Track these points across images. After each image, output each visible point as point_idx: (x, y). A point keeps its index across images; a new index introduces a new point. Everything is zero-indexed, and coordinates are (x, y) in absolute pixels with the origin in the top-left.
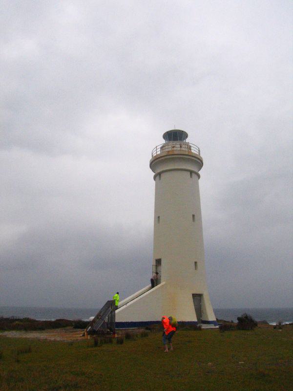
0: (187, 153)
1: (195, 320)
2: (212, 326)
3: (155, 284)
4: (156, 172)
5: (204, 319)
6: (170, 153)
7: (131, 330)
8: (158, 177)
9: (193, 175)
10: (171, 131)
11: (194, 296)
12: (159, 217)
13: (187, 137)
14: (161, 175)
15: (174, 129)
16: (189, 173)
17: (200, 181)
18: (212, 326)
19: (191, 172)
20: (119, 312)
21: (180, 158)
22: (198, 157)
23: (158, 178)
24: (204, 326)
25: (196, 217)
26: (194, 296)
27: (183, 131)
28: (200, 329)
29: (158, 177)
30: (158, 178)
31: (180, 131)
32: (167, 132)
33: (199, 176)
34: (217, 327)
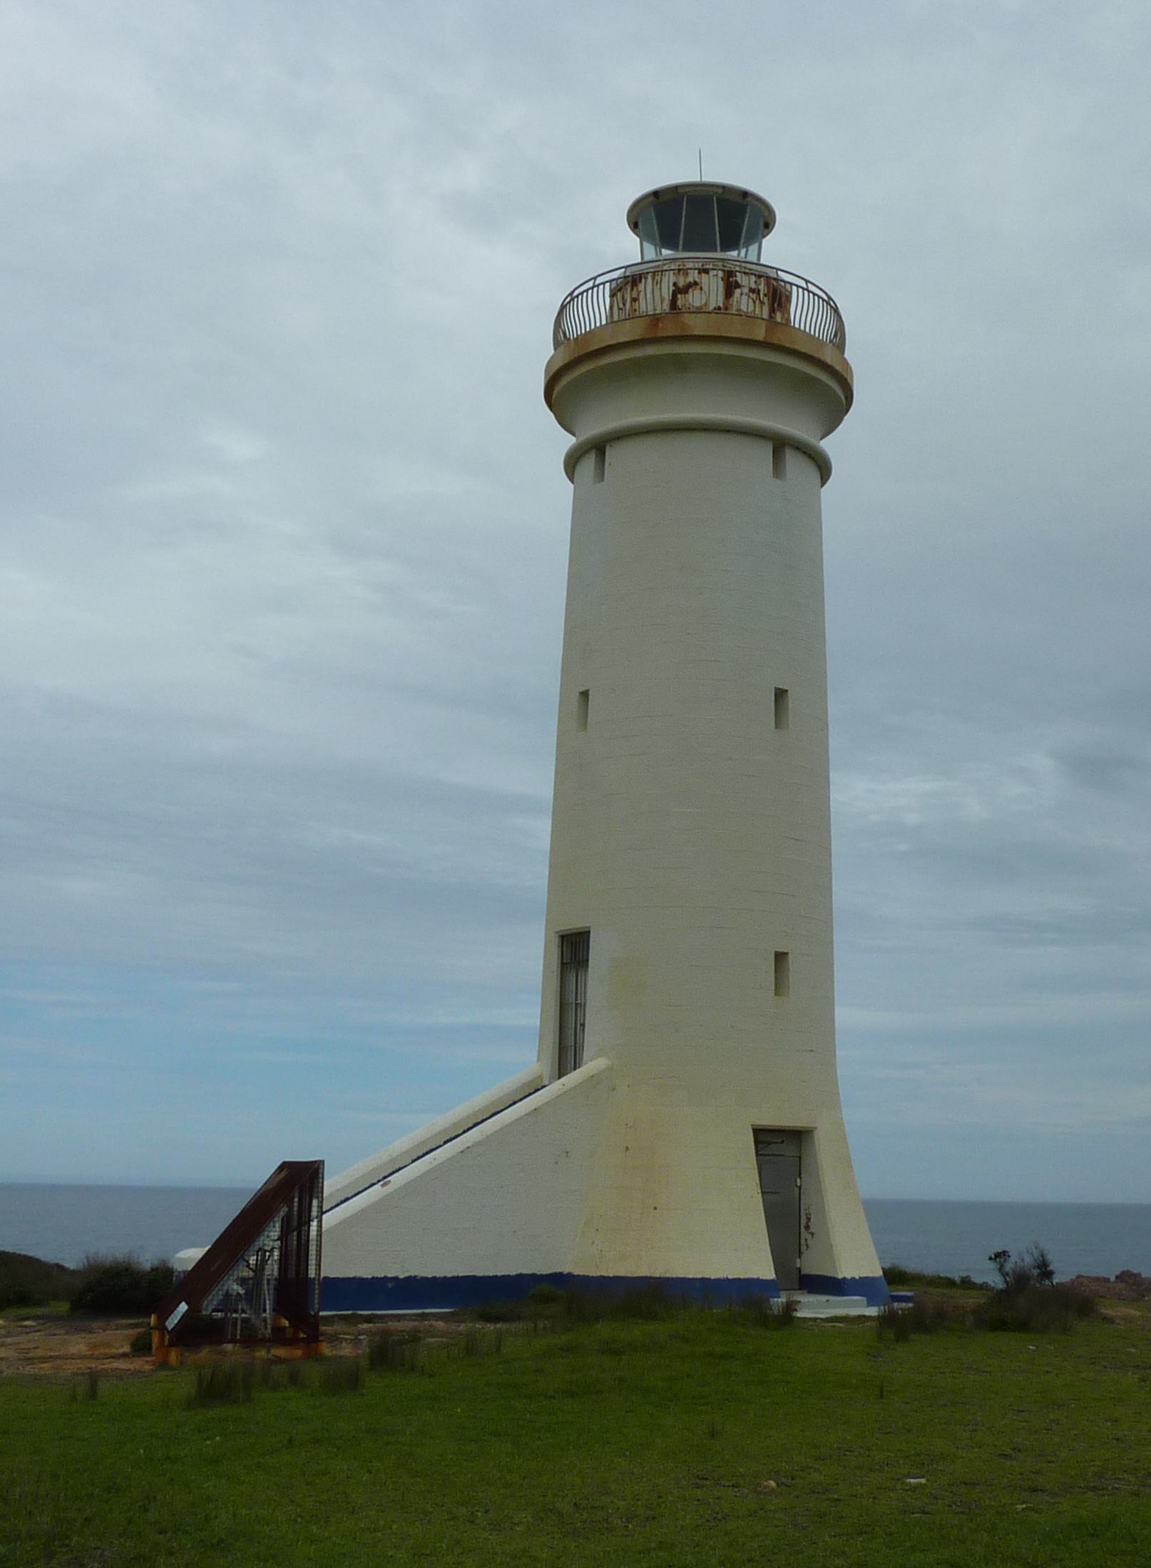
0: (760, 334)
1: (767, 1271)
2: (856, 1307)
3: (577, 1066)
4: (583, 437)
5: (811, 1265)
6: (668, 329)
7: (402, 1317)
8: (589, 463)
9: (793, 461)
10: (675, 189)
11: (763, 1136)
12: (585, 695)
13: (768, 225)
14: (610, 453)
15: (694, 178)
16: (764, 452)
17: (828, 492)
18: (856, 1307)
19: (780, 445)
20: (346, 1223)
21: (721, 363)
22: (829, 357)
23: (588, 465)
24: (812, 1307)
25: (792, 701)
26: (763, 1136)
27: (745, 194)
28: (787, 1317)
29: (589, 463)
30: (588, 465)
31: (725, 188)
32: (655, 194)
33: (823, 468)
34: (873, 1311)
